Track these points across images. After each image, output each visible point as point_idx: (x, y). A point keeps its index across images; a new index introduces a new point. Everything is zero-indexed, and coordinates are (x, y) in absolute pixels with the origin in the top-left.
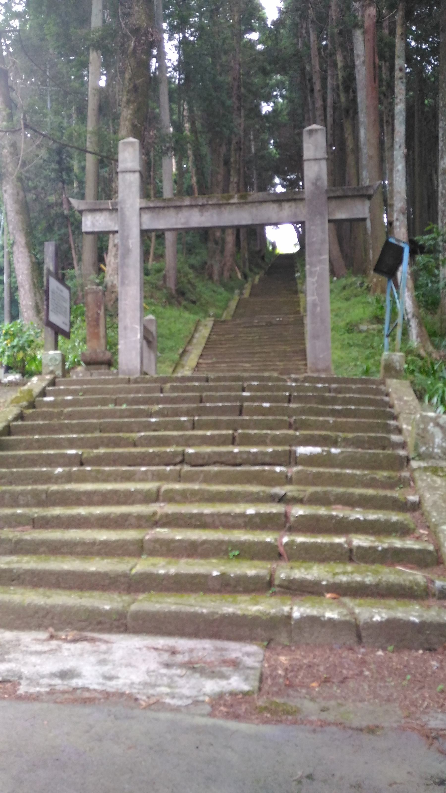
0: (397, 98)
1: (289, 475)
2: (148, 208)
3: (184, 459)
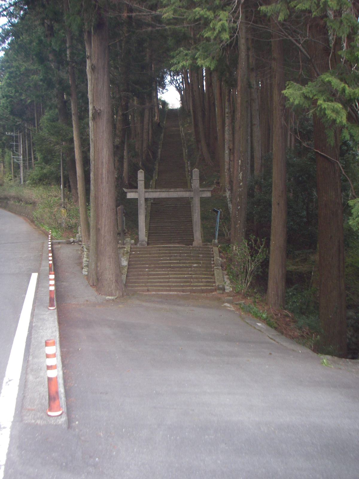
3: (170, 267)
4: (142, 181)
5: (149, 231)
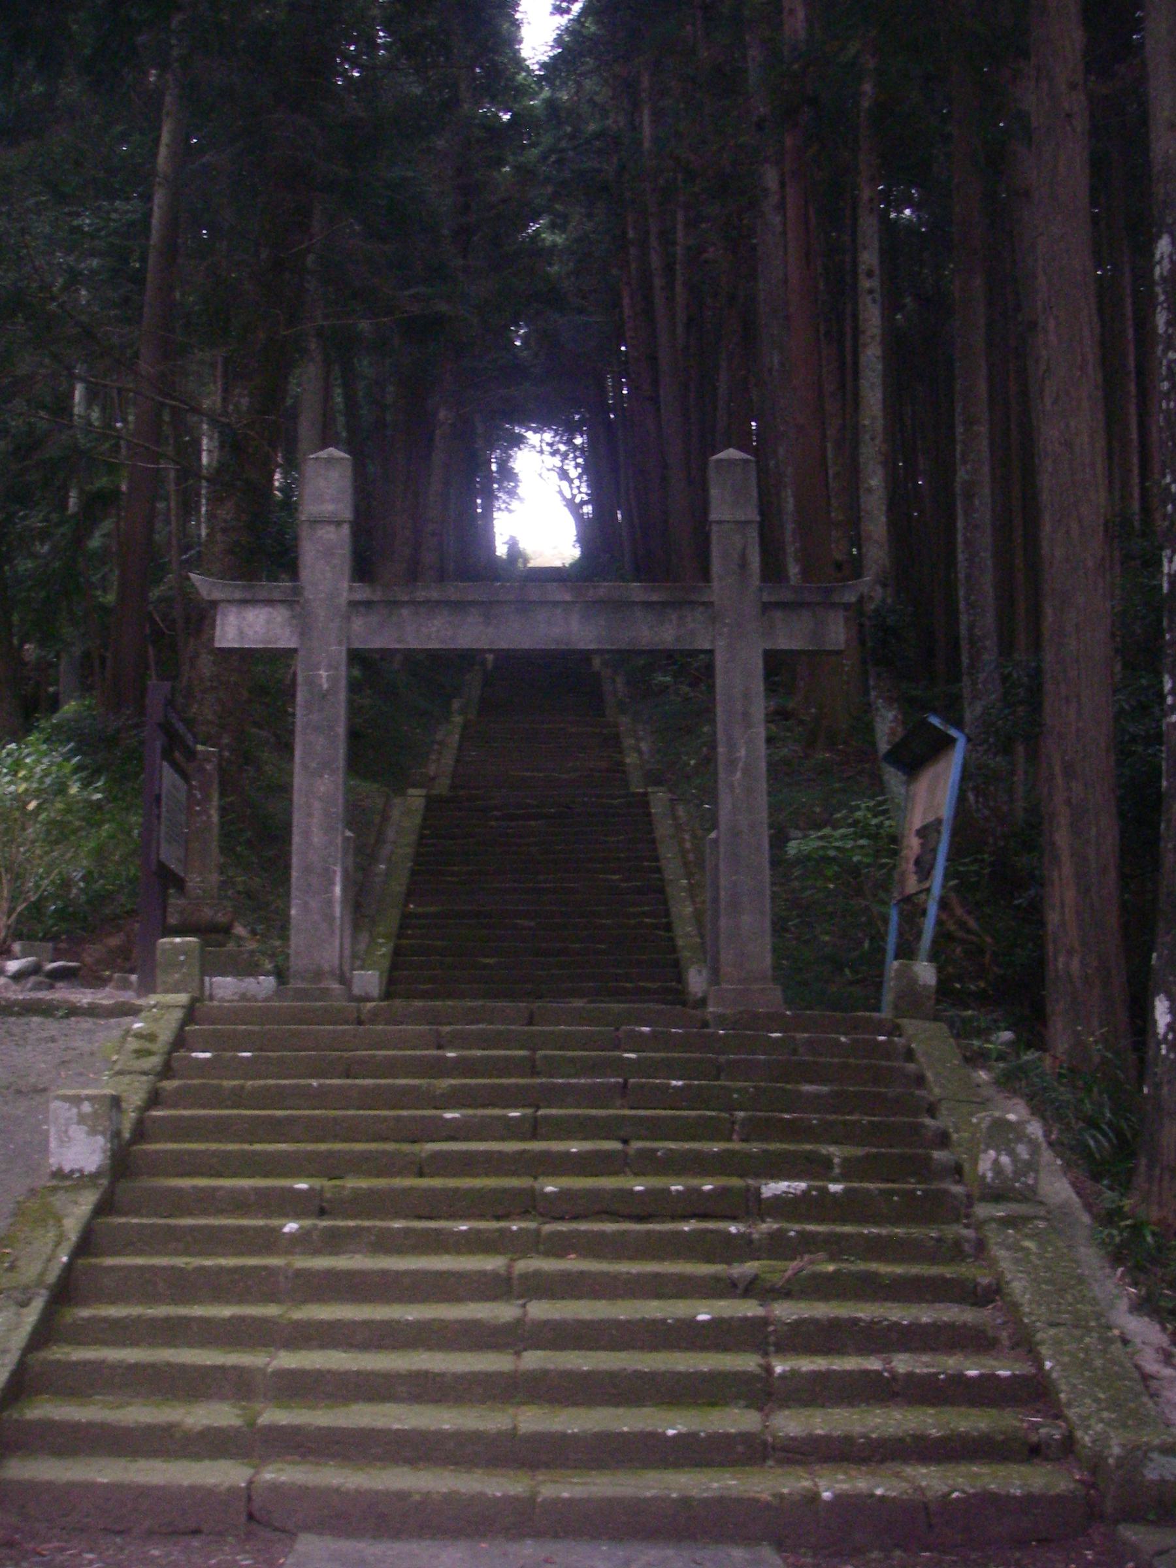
0: (863, 332)
1: (756, 1236)
2: (777, 605)
3: (530, 1204)
4: (338, 523)
5: (400, 936)
